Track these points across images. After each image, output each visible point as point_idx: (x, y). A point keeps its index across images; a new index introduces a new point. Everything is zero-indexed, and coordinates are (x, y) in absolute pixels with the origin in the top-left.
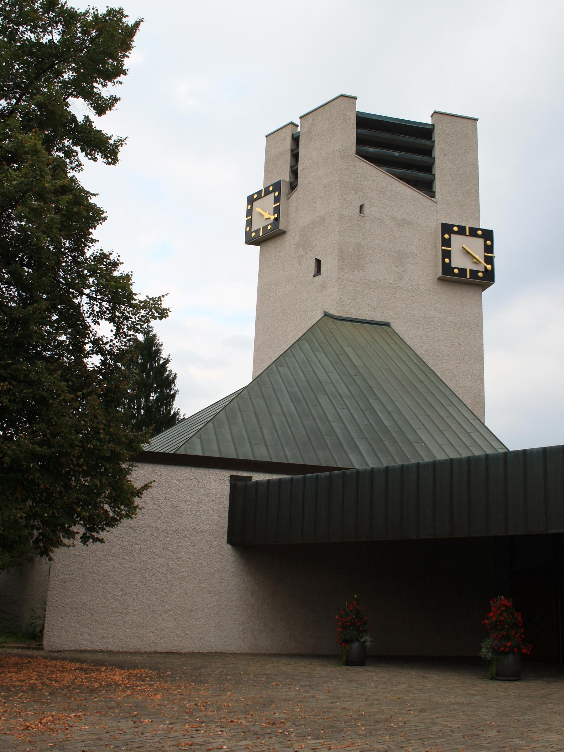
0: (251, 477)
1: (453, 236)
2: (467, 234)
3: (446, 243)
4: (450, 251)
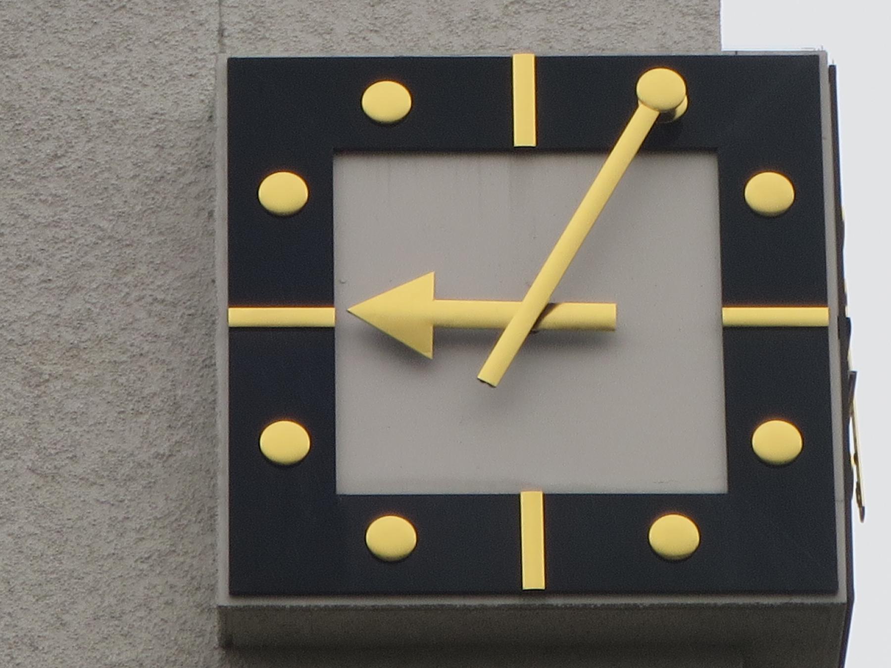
0: (438, 295)
1: (359, 183)
2: (525, 132)
3: (286, 257)
4: (734, 292)
